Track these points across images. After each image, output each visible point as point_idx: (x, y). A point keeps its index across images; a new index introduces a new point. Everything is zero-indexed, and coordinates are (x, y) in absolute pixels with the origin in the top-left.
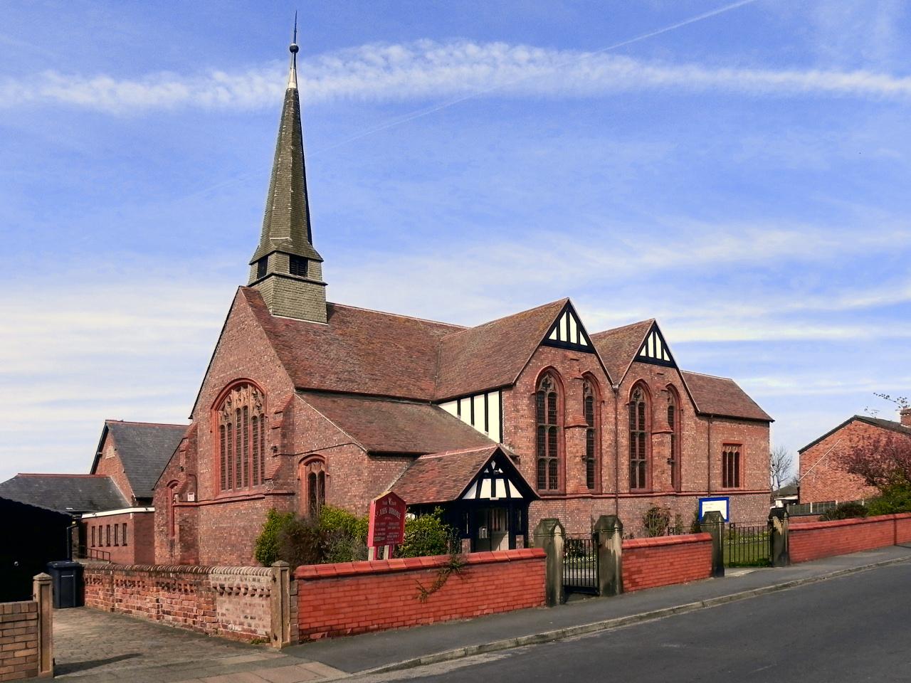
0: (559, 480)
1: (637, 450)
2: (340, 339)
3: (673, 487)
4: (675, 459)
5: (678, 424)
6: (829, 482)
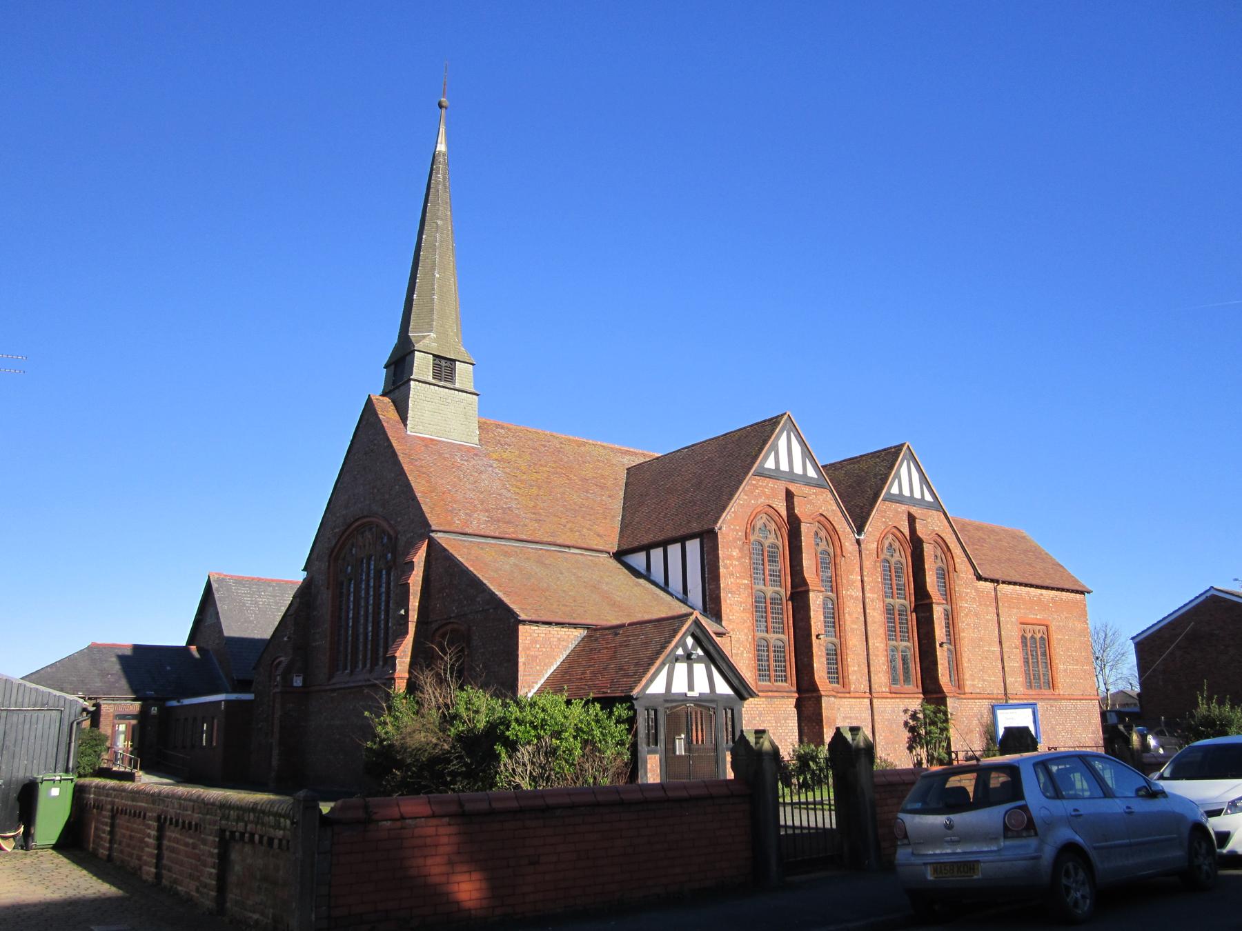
2: (495, 465)
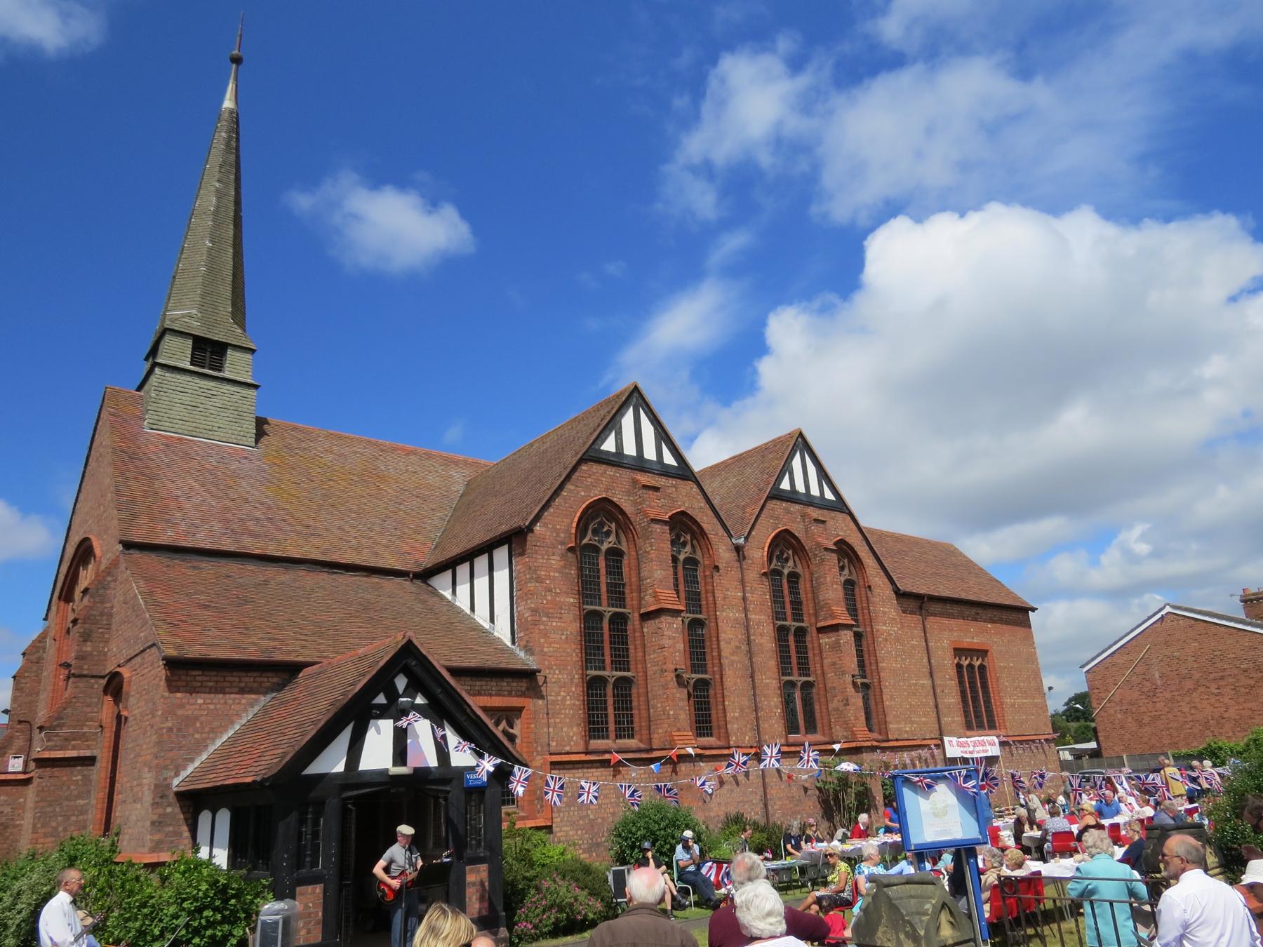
0: (636, 719)
1: (794, 660)
3: (870, 730)
4: (868, 675)
5: (866, 611)
6: (1146, 719)
